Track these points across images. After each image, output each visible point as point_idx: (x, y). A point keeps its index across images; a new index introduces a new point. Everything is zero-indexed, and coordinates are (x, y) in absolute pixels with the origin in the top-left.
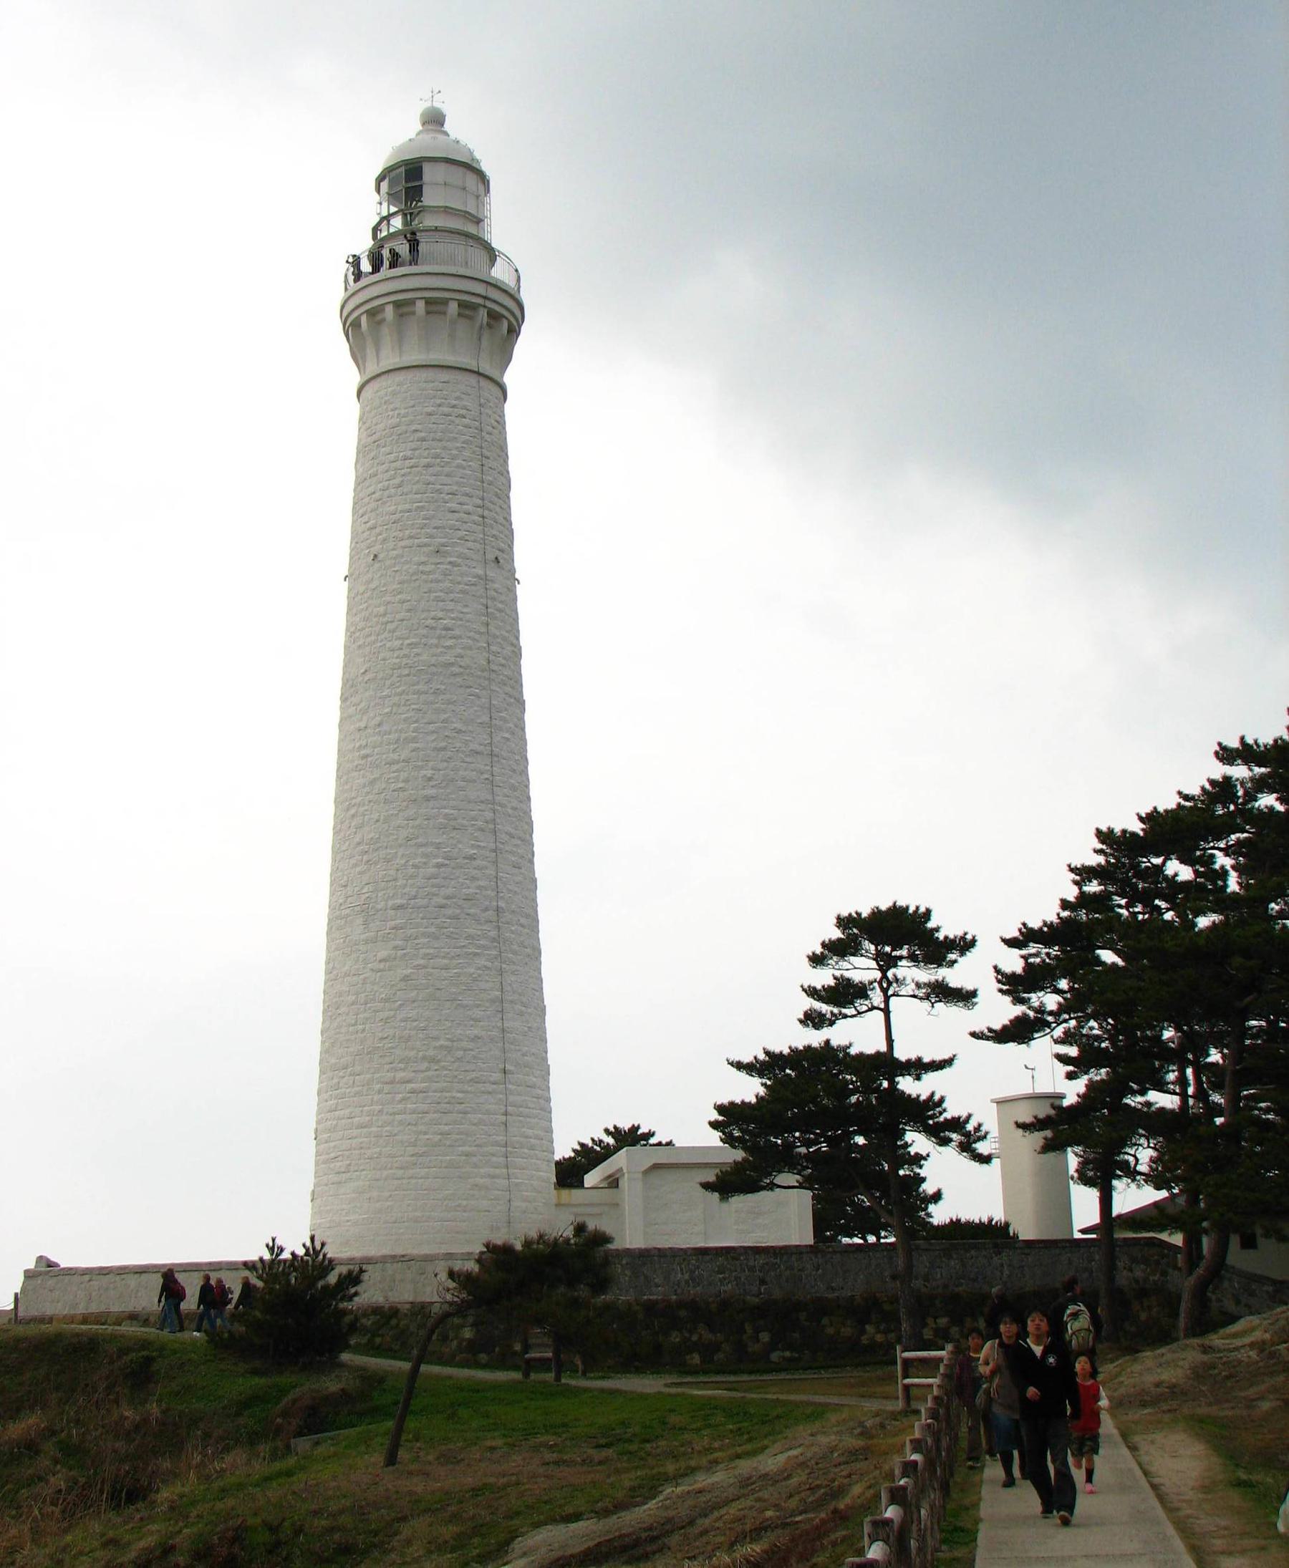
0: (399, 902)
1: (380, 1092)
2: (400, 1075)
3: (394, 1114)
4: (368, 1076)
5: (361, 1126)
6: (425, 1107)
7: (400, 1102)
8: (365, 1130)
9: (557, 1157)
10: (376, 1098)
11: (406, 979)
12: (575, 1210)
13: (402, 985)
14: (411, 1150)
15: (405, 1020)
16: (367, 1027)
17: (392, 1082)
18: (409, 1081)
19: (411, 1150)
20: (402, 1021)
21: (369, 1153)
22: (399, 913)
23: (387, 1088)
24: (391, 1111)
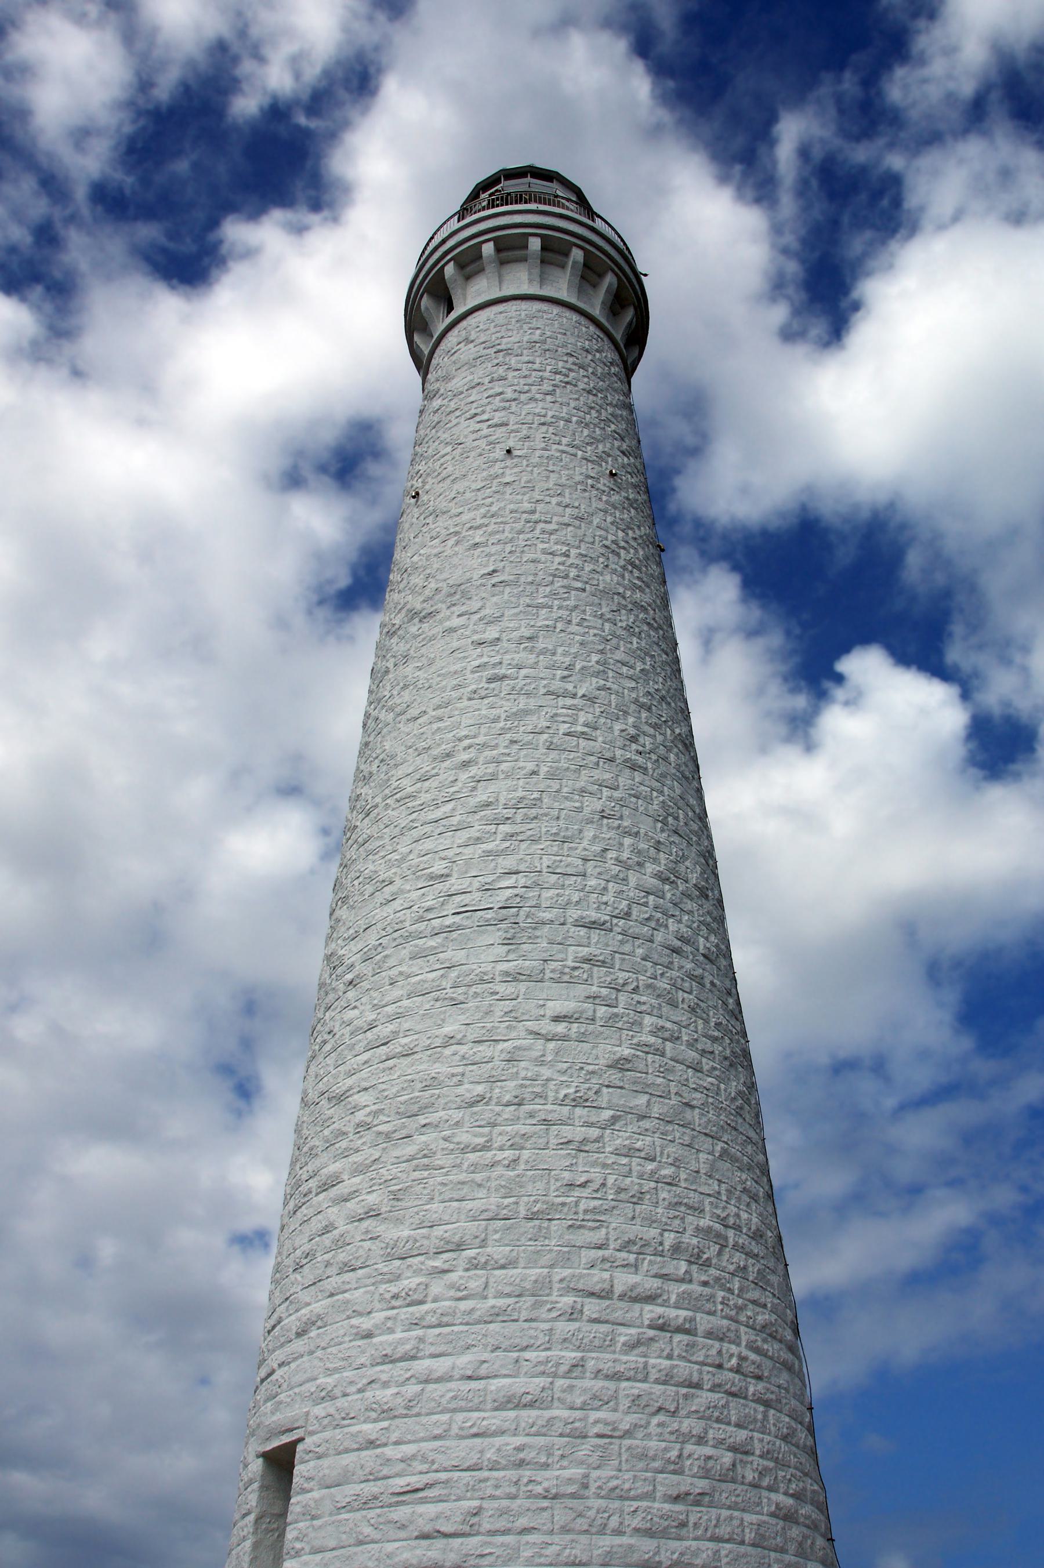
0: (594, 915)
1: (573, 1314)
2: (624, 1280)
3: (616, 1377)
4: (534, 1273)
5: (511, 1402)
6: (684, 1369)
7: (632, 1346)
8: (529, 1415)
9: (378, 618)
10: (564, 1327)
11: (620, 1065)
12: (590, 222)
13: (614, 1076)
14: (668, 1483)
15: (629, 1152)
16: (526, 1154)
17: (604, 1294)
18: (650, 1299)
19: (668, 1483)
20: (616, 1153)
21: (548, 1479)
22: (595, 935)
23: (592, 1307)
24: (607, 1367)
